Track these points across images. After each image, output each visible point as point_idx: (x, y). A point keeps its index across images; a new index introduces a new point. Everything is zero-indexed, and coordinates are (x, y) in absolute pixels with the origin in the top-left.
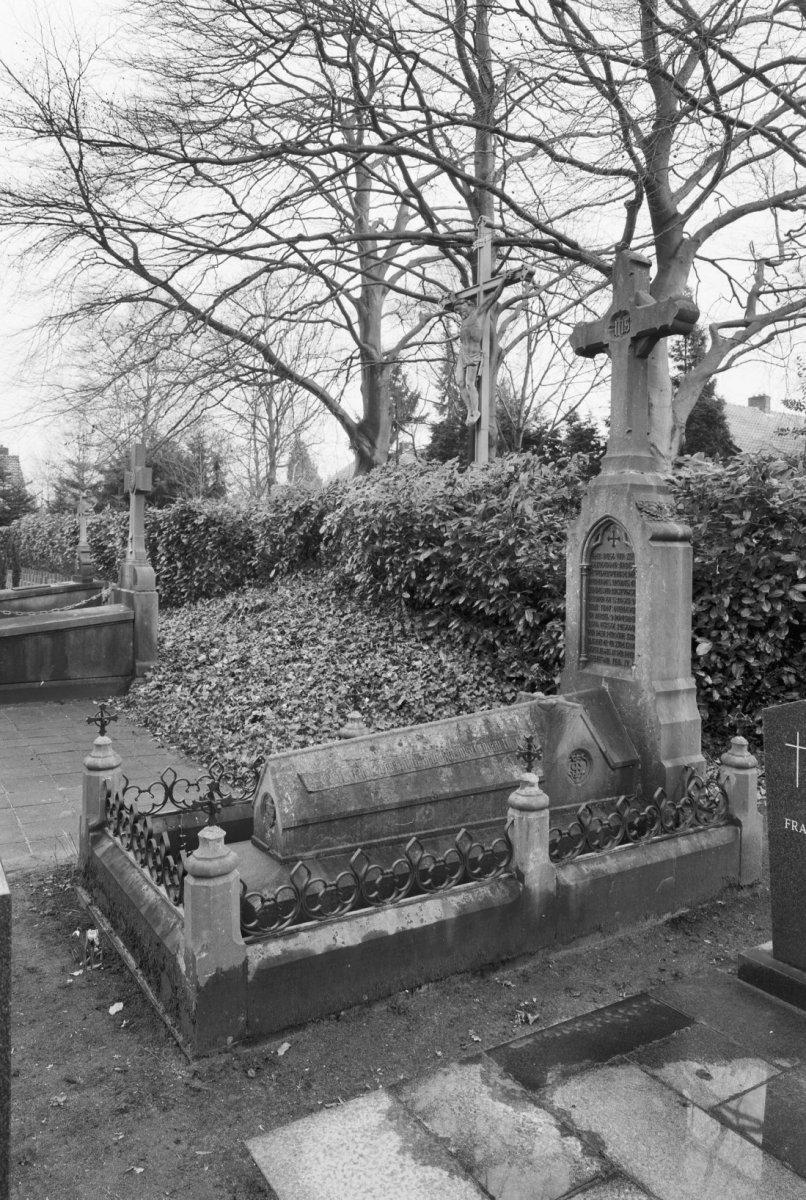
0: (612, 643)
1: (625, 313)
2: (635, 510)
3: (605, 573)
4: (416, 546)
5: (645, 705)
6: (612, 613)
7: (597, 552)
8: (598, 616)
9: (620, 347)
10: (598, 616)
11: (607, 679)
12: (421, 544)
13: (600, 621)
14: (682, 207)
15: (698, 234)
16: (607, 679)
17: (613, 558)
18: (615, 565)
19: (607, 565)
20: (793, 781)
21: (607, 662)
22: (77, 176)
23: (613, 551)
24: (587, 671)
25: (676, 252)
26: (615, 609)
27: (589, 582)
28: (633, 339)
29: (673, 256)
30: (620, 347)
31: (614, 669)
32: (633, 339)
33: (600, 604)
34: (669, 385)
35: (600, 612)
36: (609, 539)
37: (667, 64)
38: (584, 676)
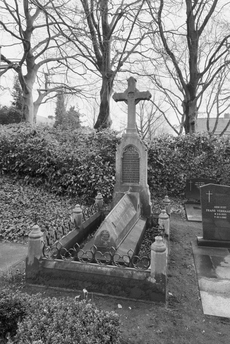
0: (131, 177)
1: (133, 93)
2: (140, 143)
3: (128, 159)
4: (9, 152)
5: (144, 191)
6: (131, 169)
7: (125, 153)
8: (125, 170)
9: (131, 101)
10: (125, 170)
11: (131, 186)
12: (11, 151)
13: (127, 172)
14: (34, 54)
15: (39, 63)
16: (131, 186)
17: (131, 155)
18: (132, 157)
19: (129, 157)
20: (208, 201)
21: (129, 182)
22: (145, 28)
23: (131, 153)
24: (123, 185)
25: (33, 67)
26: (132, 168)
27: (123, 161)
28: (136, 100)
29: (33, 68)
30: (131, 101)
31: (132, 184)
32: (136, 100)
33: (126, 167)
34: (33, 105)
35: (126, 169)
36: (129, 150)
37: (30, 9)
38: (122, 186)
